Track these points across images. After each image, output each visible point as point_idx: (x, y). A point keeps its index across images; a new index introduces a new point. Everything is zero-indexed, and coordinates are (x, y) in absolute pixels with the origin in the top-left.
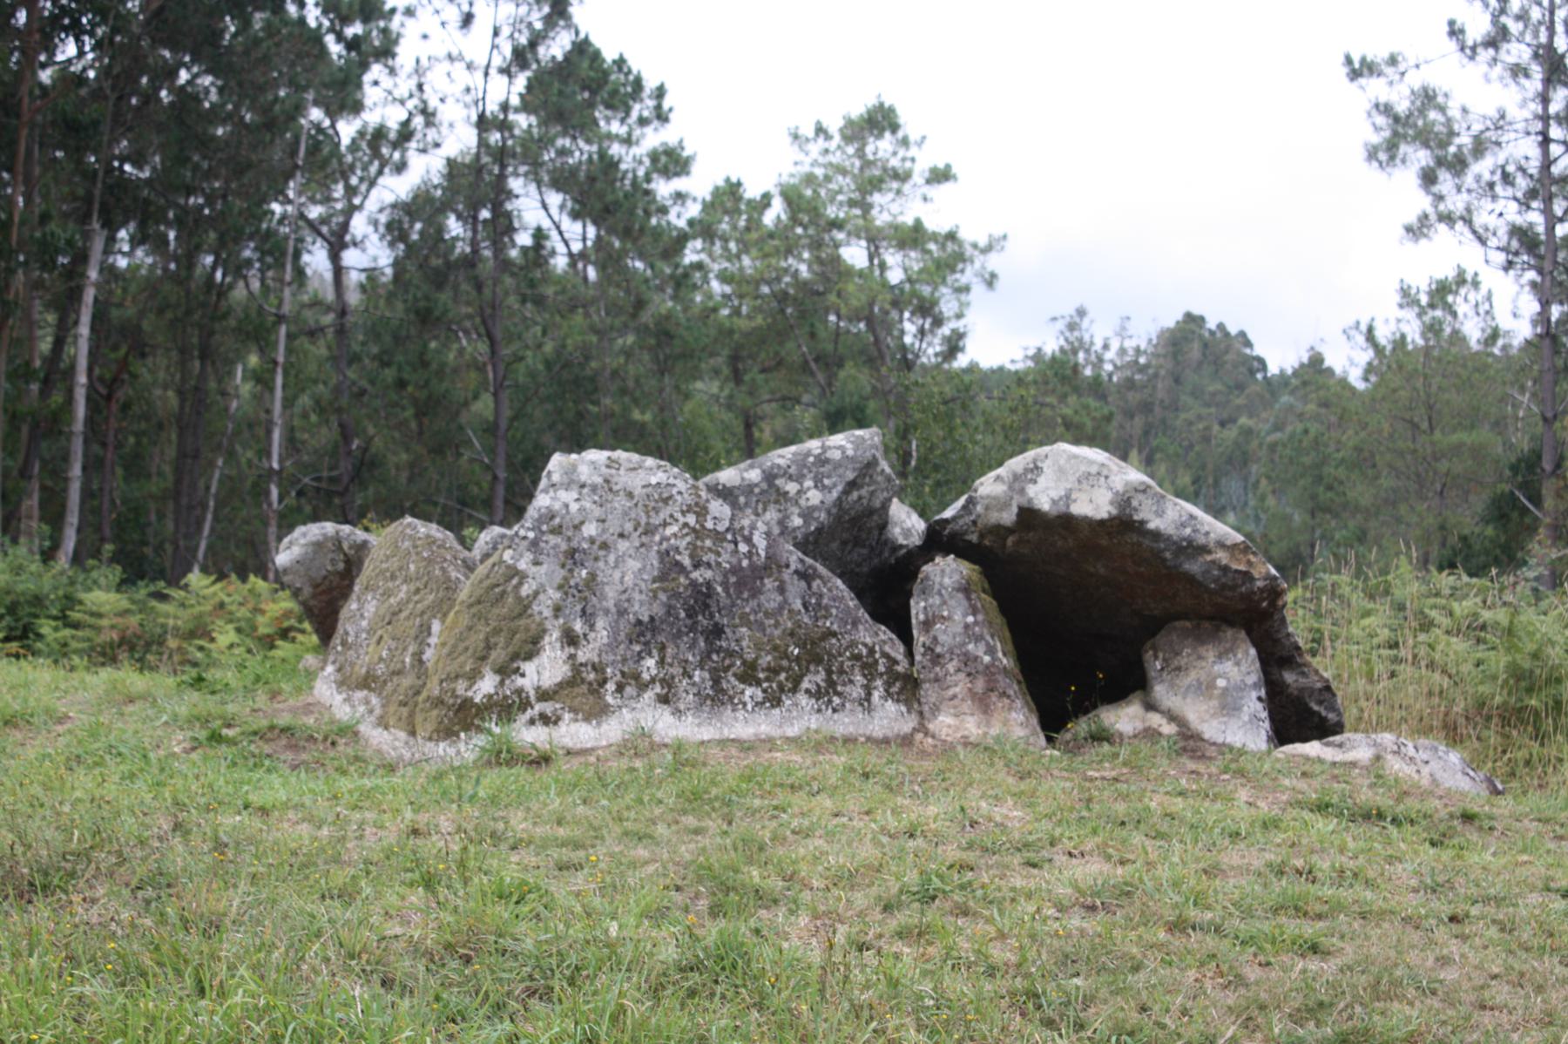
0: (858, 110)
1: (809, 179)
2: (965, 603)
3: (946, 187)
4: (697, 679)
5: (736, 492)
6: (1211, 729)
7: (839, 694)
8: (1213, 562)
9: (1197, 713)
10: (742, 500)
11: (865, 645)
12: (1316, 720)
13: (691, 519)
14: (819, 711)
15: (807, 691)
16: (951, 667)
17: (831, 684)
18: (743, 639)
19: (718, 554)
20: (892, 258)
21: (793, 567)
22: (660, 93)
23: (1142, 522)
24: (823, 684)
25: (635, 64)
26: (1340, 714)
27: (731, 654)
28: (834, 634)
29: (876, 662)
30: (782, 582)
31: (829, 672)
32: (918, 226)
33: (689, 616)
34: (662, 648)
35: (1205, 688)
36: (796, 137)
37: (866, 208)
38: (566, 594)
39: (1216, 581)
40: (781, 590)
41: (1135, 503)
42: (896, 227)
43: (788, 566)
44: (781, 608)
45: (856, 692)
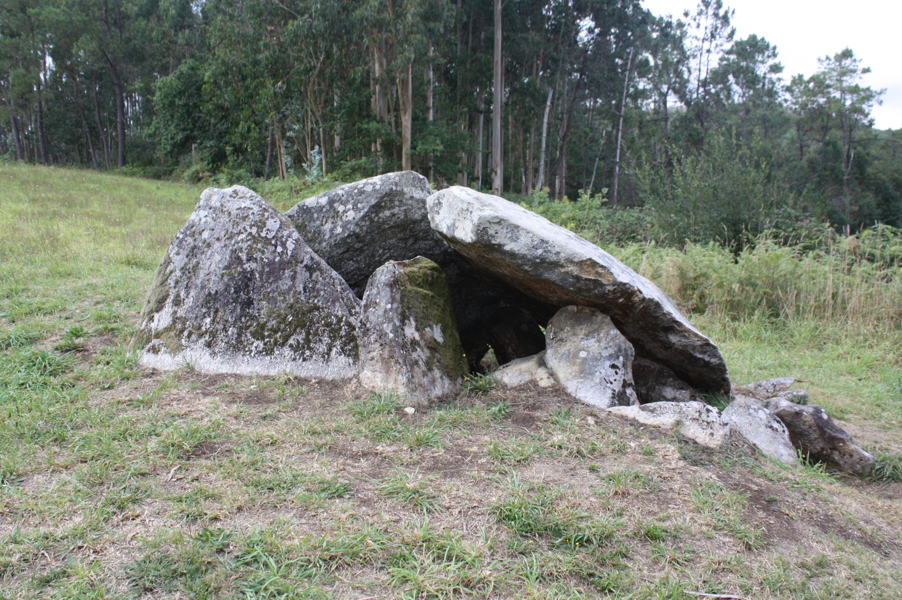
0: (840, 52)
1: (824, 73)
2: (389, 294)
3: (867, 74)
4: (230, 333)
5: (313, 211)
6: (572, 386)
7: (310, 349)
8: (567, 273)
9: (565, 373)
10: (315, 215)
11: (336, 316)
12: (702, 363)
13: (254, 231)
14: (294, 359)
15: (291, 346)
16: (372, 339)
17: (307, 341)
18: (262, 309)
19: (263, 253)
20: (848, 97)
21: (305, 263)
22: (775, 48)
23: (500, 246)
24: (302, 342)
25: (767, 40)
26: (721, 359)
27: (253, 318)
28: (317, 308)
29: (340, 328)
30: (295, 273)
31: (308, 334)
32: (857, 86)
33: (235, 292)
34: (217, 311)
35: (571, 357)
36: (819, 60)
37: (841, 81)
38: (183, 273)
39: (573, 285)
40: (293, 278)
41: (491, 232)
42: (850, 87)
43: (302, 262)
44: (290, 289)
45: (322, 348)
